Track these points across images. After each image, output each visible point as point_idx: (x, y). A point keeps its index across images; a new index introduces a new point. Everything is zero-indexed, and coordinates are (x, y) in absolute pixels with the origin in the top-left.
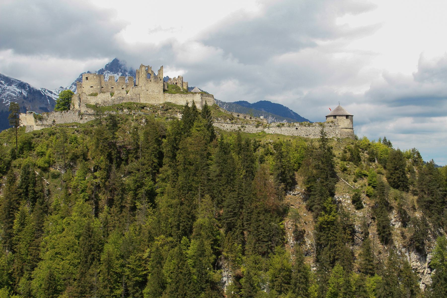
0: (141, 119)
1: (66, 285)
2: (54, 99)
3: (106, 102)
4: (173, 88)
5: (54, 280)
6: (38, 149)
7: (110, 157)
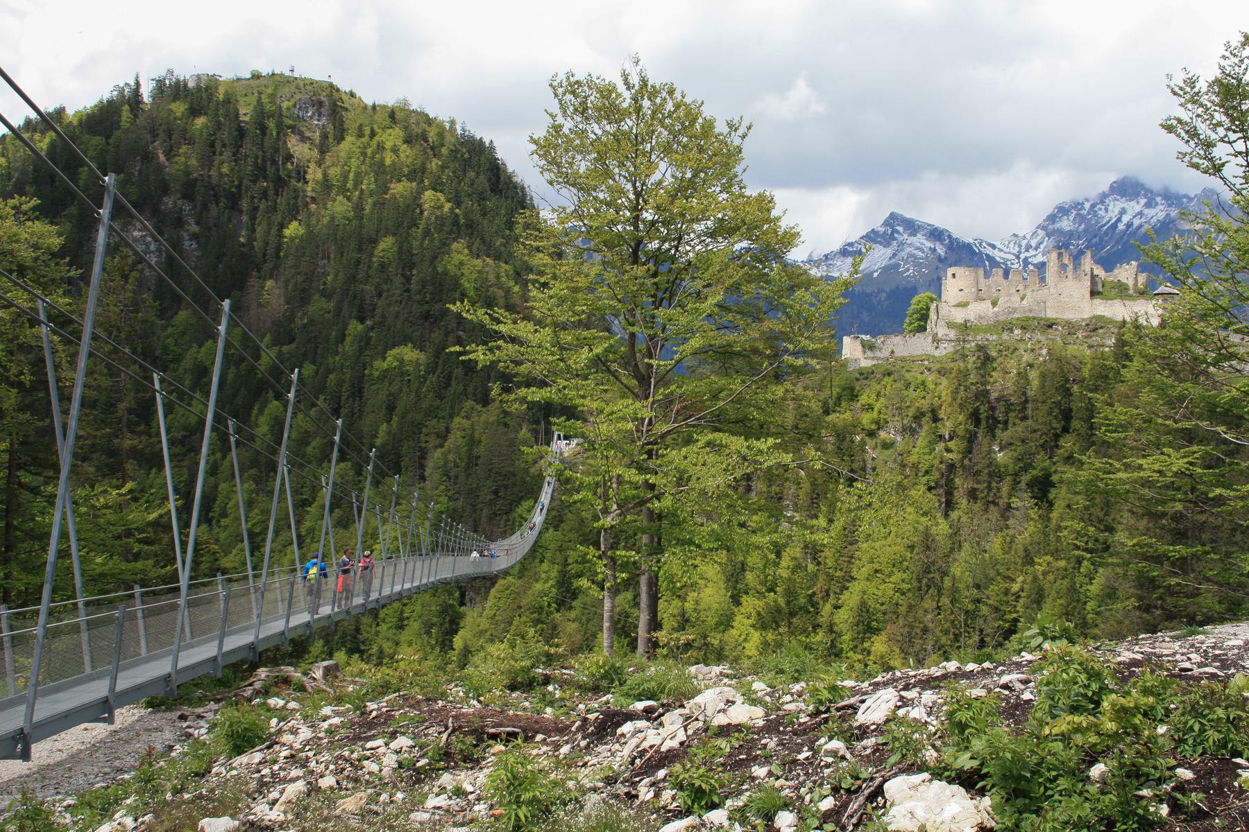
0: (1041, 348)
1: (885, 622)
2: (998, 259)
4: (1113, 288)
5: (868, 611)
6: (864, 399)
7: (975, 417)
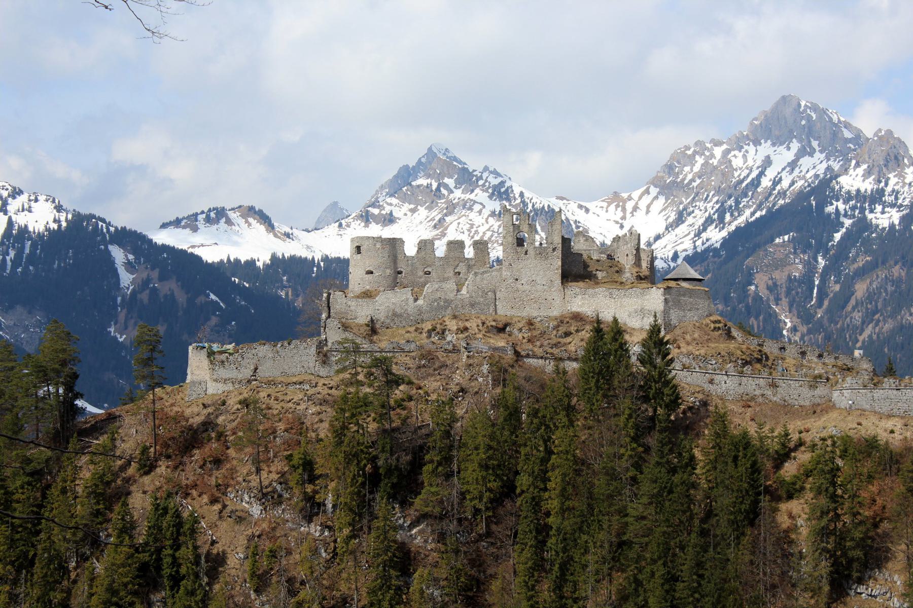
3: (401, 315)
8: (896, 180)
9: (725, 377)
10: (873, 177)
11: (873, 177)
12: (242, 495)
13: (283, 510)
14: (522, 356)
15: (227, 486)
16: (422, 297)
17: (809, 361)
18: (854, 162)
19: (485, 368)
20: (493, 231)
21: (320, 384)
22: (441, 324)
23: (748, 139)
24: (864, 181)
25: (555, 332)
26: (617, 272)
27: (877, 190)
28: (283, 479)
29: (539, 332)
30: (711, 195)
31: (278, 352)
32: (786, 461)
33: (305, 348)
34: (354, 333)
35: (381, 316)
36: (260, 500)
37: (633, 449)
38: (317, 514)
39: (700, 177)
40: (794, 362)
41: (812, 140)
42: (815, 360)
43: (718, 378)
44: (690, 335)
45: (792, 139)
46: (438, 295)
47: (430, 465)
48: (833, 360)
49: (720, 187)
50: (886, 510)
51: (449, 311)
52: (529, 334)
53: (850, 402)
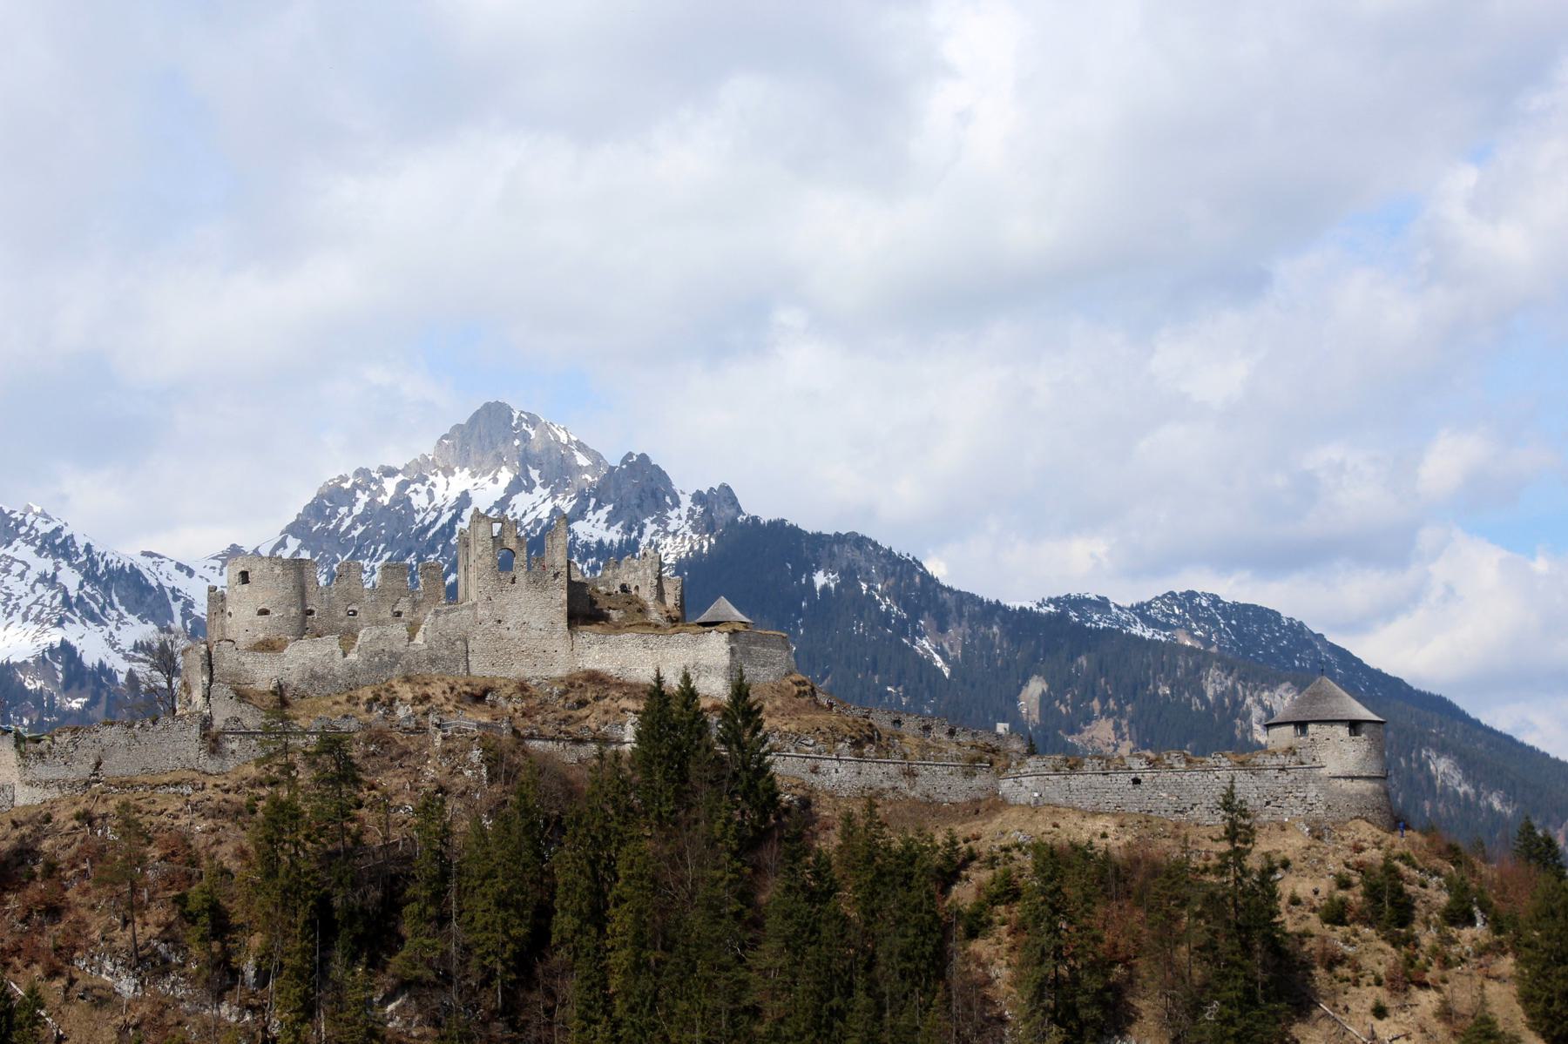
3: (323, 678)
7: (324, 924)
8: (655, 527)
9: (836, 764)
10: (622, 523)
11: (622, 523)
12: (101, 962)
13: (174, 984)
14: (523, 737)
15: (75, 948)
16: (356, 649)
17: (935, 740)
18: (593, 501)
19: (476, 755)
20: (43, 605)
21: (209, 785)
22: (387, 690)
23: (436, 467)
24: (608, 528)
25: (562, 701)
26: (640, 611)
27: (628, 541)
28: (168, 933)
29: (538, 701)
30: (380, 548)
31: (135, 736)
32: (953, 883)
33: (182, 730)
34: (255, 706)
35: (293, 679)
36: (134, 969)
37: (735, 871)
38: (231, 988)
39: (363, 524)
40: (916, 741)
41: (530, 468)
42: (945, 738)
43: (824, 765)
44: (770, 703)
45: (501, 466)
46: (381, 646)
47: (415, 904)
48: (969, 738)
49: (394, 537)
50: (1119, 949)
51: (397, 671)
52: (524, 704)
53: (1036, 795)
